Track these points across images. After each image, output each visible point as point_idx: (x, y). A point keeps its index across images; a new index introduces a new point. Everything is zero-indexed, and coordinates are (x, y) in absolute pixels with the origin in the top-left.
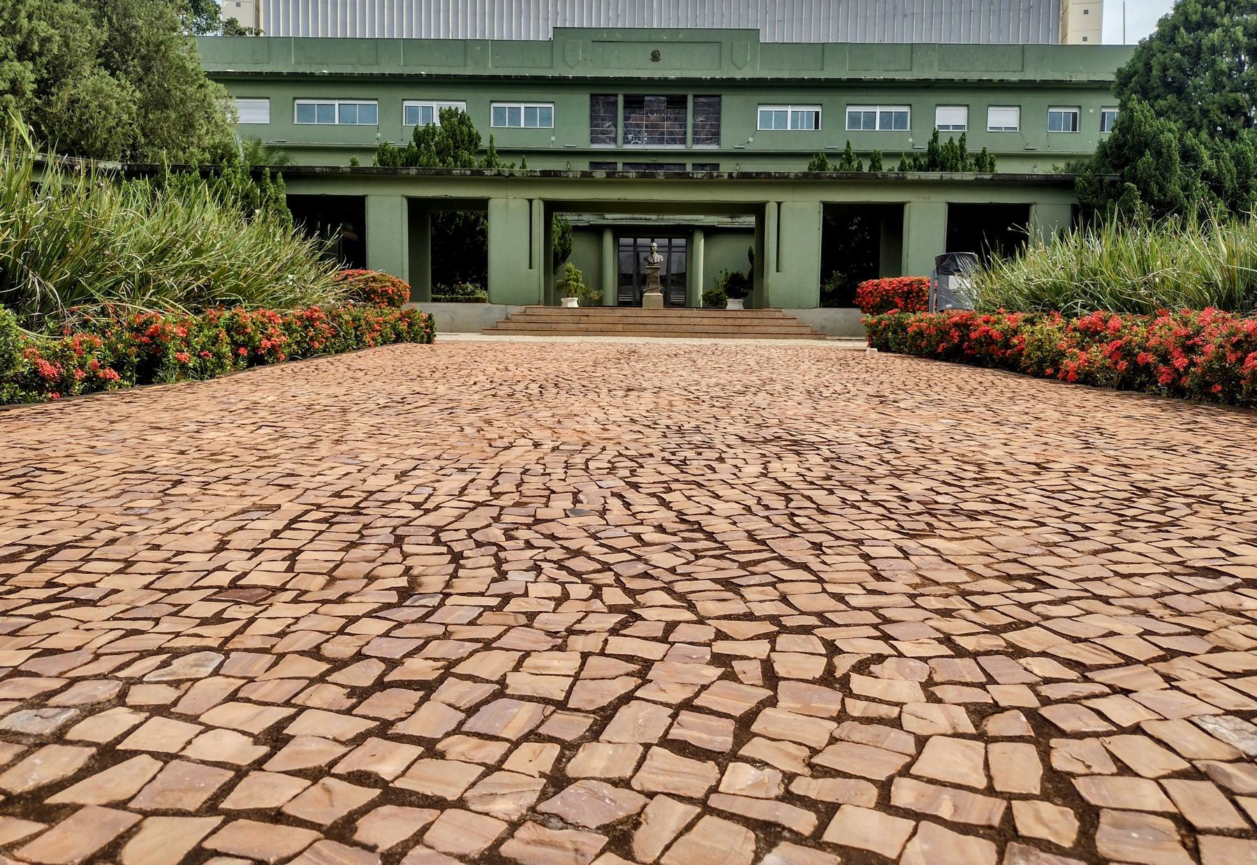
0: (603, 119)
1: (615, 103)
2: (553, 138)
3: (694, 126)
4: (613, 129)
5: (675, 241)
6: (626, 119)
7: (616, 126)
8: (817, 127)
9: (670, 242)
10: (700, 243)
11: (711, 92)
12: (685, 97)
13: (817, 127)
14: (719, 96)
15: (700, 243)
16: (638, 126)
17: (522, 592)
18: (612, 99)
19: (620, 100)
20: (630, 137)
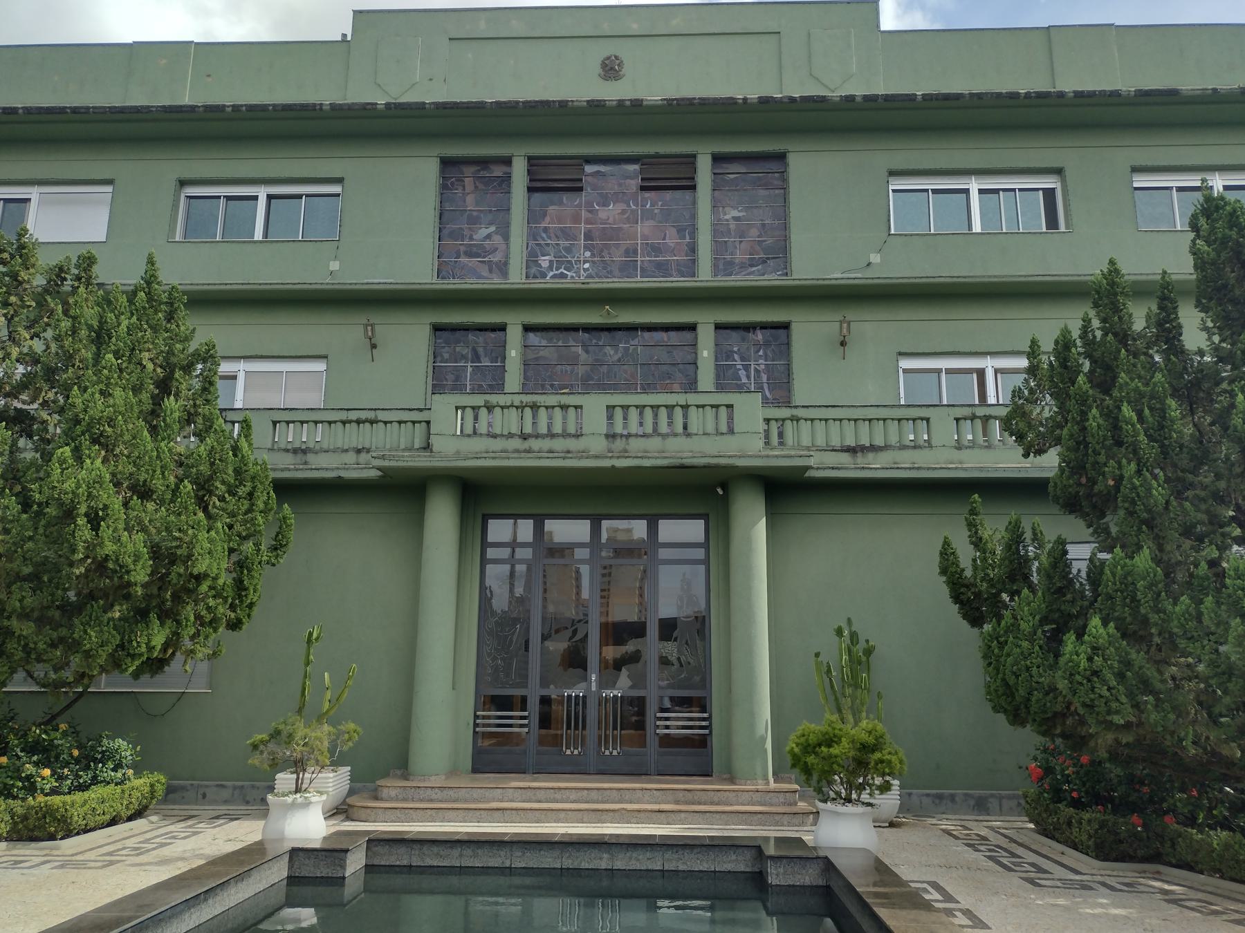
0: (474, 221)
1: (507, 178)
2: (335, 266)
3: (718, 230)
4: (498, 239)
5: (670, 530)
6: (533, 217)
7: (506, 238)
8: (1052, 222)
9: (653, 530)
10: (753, 528)
11: (758, 137)
12: (690, 161)
13: (1052, 222)
14: (781, 157)
15: (753, 528)
16: (566, 234)
17: (962, 422)
18: (498, 171)
19: (519, 170)
20: (544, 261)
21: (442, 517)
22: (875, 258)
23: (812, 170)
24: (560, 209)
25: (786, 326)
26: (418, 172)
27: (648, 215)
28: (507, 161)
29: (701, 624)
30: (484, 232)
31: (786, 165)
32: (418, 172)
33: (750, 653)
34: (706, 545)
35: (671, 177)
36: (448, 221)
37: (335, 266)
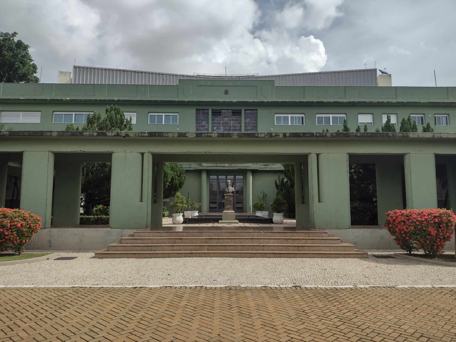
0: (202, 120)
1: (208, 113)
2: (178, 129)
4: (206, 124)
6: (213, 120)
7: (208, 124)
14: (257, 110)
16: (219, 123)
18: (206, 111)
20: (215, 128)
21: (204, 176)
22: (272, 129)
23: (262, 113)
24: (217, 119)
25: (257, 110)
26: (192, 111)
27: (233, 120)
28: (208, 110)
29: (242, 192)
30: (204, 123)
31: (257, 113)
32: (192, 111)
33: (249, 191)
34: (243, 180)
35: (237, 113)
36: (198, 121)
37: (178, 129)
